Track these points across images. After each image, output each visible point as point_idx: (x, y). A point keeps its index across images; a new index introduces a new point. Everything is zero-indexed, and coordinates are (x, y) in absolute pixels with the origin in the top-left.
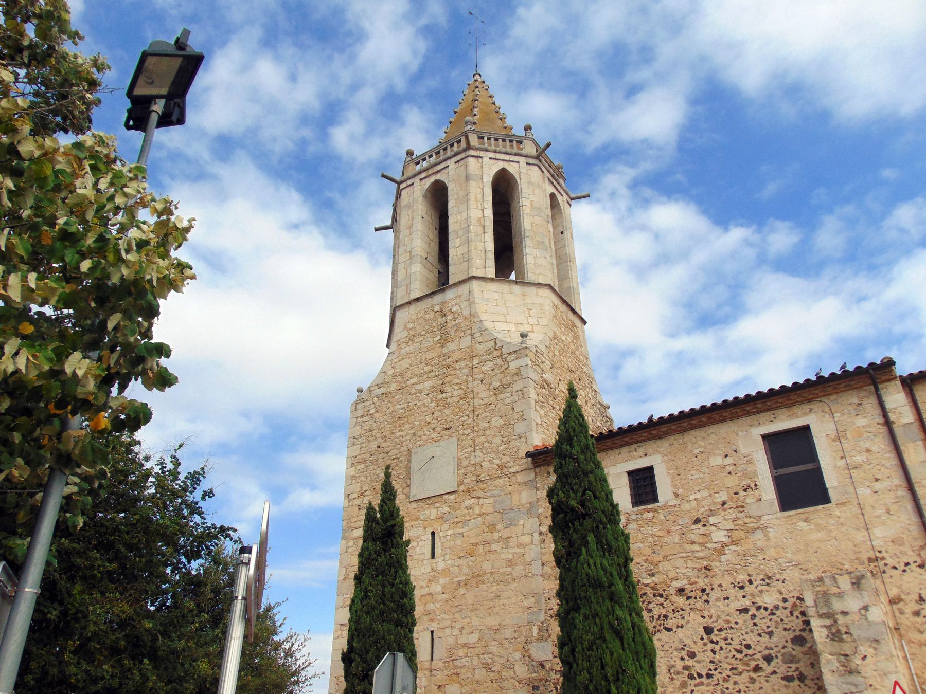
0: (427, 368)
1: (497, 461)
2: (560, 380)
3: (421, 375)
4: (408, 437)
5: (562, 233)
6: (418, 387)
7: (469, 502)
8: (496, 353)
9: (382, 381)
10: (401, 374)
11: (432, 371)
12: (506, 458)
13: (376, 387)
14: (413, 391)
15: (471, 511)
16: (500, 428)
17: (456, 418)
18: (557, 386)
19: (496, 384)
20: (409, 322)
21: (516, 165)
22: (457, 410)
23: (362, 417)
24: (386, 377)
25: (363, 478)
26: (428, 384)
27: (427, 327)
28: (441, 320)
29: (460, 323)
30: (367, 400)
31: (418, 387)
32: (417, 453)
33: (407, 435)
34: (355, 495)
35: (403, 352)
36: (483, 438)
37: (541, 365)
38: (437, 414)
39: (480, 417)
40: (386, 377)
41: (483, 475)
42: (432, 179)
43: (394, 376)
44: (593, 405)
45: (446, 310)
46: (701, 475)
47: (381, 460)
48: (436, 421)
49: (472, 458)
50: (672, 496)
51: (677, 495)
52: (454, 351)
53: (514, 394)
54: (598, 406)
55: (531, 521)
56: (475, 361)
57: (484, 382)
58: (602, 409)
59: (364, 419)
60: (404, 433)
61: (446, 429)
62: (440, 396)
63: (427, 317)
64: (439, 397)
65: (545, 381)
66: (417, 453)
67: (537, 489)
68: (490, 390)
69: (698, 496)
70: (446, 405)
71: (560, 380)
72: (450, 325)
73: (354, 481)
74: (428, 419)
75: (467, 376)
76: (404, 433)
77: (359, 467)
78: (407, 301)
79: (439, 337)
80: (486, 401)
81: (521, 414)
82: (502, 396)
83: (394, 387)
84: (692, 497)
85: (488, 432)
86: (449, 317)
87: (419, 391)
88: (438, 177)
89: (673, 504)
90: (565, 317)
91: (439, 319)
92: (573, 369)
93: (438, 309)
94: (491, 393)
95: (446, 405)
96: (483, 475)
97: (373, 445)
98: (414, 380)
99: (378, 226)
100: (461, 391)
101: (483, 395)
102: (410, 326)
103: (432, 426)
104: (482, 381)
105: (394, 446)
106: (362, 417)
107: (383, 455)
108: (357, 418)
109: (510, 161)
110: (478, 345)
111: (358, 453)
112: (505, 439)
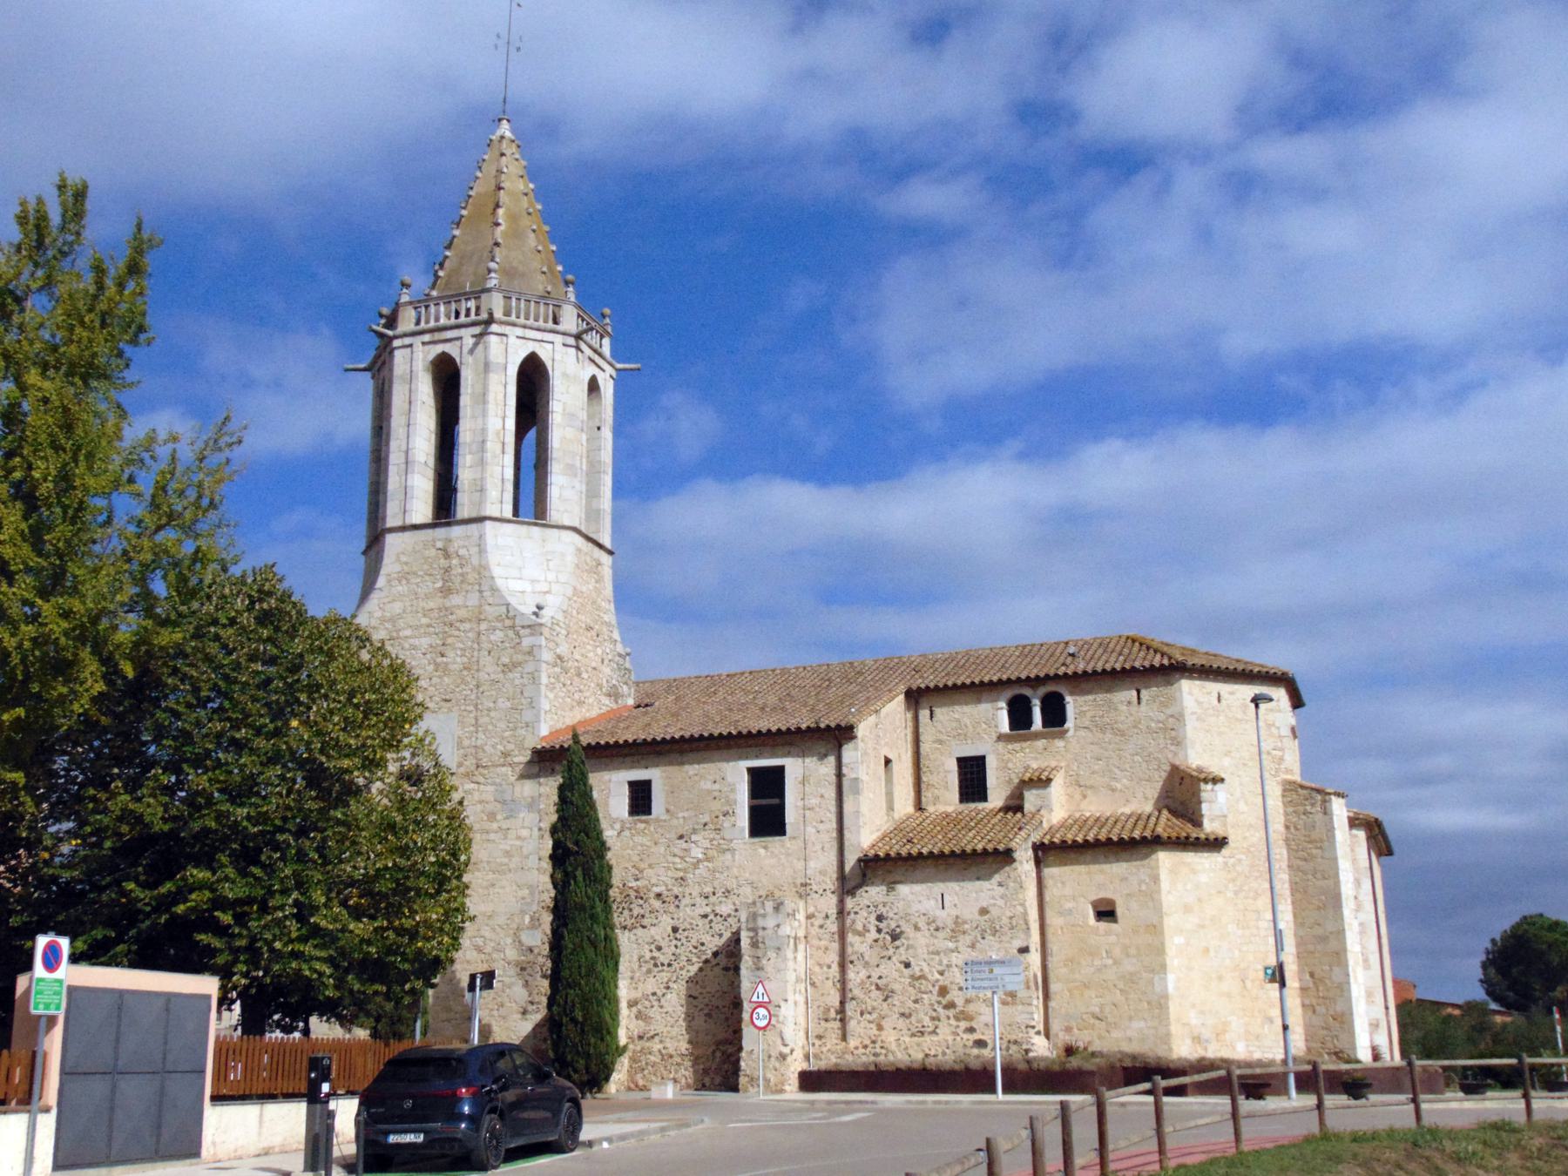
3: (417, 627)
19: (506, 660)
31: (416, 642)
38: (435, 680)
42: (439, 349)
45: (451, 550)
51: (668, 811)
84: (680, 815)
102: (404, 559)
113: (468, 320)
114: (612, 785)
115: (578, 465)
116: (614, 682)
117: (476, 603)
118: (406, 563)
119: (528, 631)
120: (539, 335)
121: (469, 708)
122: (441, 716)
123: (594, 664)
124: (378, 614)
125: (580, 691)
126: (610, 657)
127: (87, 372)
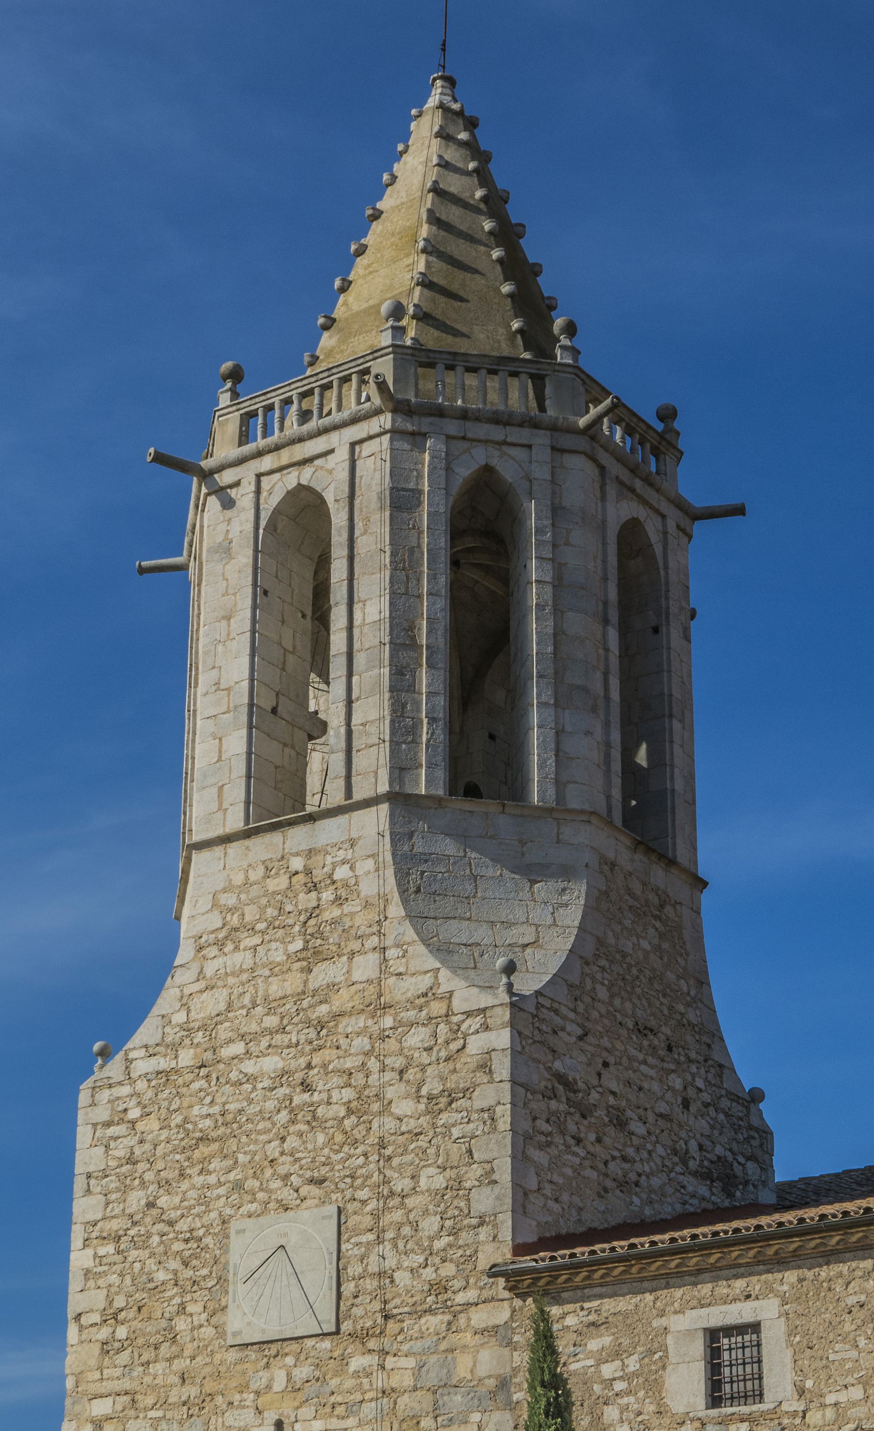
0: (272, 1021)
1: (428, 1274)
2: (606, 1065)
3: (255, 1037)
4: (222, 1191)
5: (656, 630)
6: (249, 1067)
7: (357, 1362)
8: (437, 1008)
9: (158, 1041)
10: (203, 1027)
11: (283, 1030)
12: (449, 1270)
13: (142, 1053)
14: (234, 1076)
15: (365, 1381)
16: (439, 1195)
17: (335, 1157)
18: (595, 1082)
19: (432, 1086)
20: (224, 890)
21: (519, 453)
22: (339, 1138)
23: (108, 1124)
24: (168, 1030)
25: (114, 1279)
26: (271, 1063)
27: (271, 912)
28: (306, 900)
29: (352, 915)
30: (120, 1083)
31: (249, 1067)
32: (243, 1231)
33: (220, 1184)
34: (96, 1318)
35: (210, 969)
36: (397, 1216)
37: (551, 1039)
38: (292, 1142)
39: (396, 1162)
40: (168, 1030)
41: (397, 1301)
42: (291, 480)
43: (187, 1029)
44: (707, 1105)
45: (319, 874)
46: (854, 1354)
47: (156, 1239)
48: (289, 1159)
49: (373, 1259)
50: (789, 1390)
51: (801, 1392)
52: (333, 987)
53: (475, 1116)
54: (725, 1103)
55: (497, 1416)
56: (388, 1021)
57: (405, 1077)
58: (737, 1110)
59: (112, 1131)
60: (212, 1179)
61: (311, 1181)
62: (300, 1098)
63: (273, 885)
64: (297, 1100)
65: (560, 1078)
66: (243, 1231)
67: (510, 1344)
68: (418, 1098)
69: (842, 1397)
70: (314, 1121)
71: (606, 1065)
72: (327, 915)
73: (91, 1283)
74: (273, 1149)
75: (367, 1054)
76: (212, 1179)
77: (102, 1251)
78: (219, 832)
79: (299, 944)
80: (412, 1124)
81: (488, 1167)
82: (444, 1118)
83: (186, 1058)
84: (830, 1399)
85: (410, 1202)
86: (327, 895)
87: (252, 1079)
88: (306, 476)
89: (792, 1409)
90: (637, 887)
91: (302, 896)
92: (653, 1023)
93: (300, 868)
94: (422, 1107)
95: (314, 1121)
96: (397, 1301)
97: (136, 1200)
98: (238, 1048)
99: (170, 451)
100: (348, 1094)
101: (398, 1109)
102: (229, 900)
103: (282, 1170)
104: (401, 1072)
105: (190, 1208)
106: (108, 1124)
107: (160, 1227)
108: (95, 1125)
109: (505, 443)
110: (392, 980)
111: (99, 1216)
112: (448, 1223)
113: (345, 414)
114: (670, 1340)
115: (598, 688)
116: (719, 1150)
117: (374, 974)
118: (231, 910)
119: (475, 1023)
120: (498, 433)
121: (362, 1194)
122: (305, 1214)
123: (662, 1108)
124: (180, 1017)
125: (624, 1159)
126: (706, 1097)
127: (311, 738)
